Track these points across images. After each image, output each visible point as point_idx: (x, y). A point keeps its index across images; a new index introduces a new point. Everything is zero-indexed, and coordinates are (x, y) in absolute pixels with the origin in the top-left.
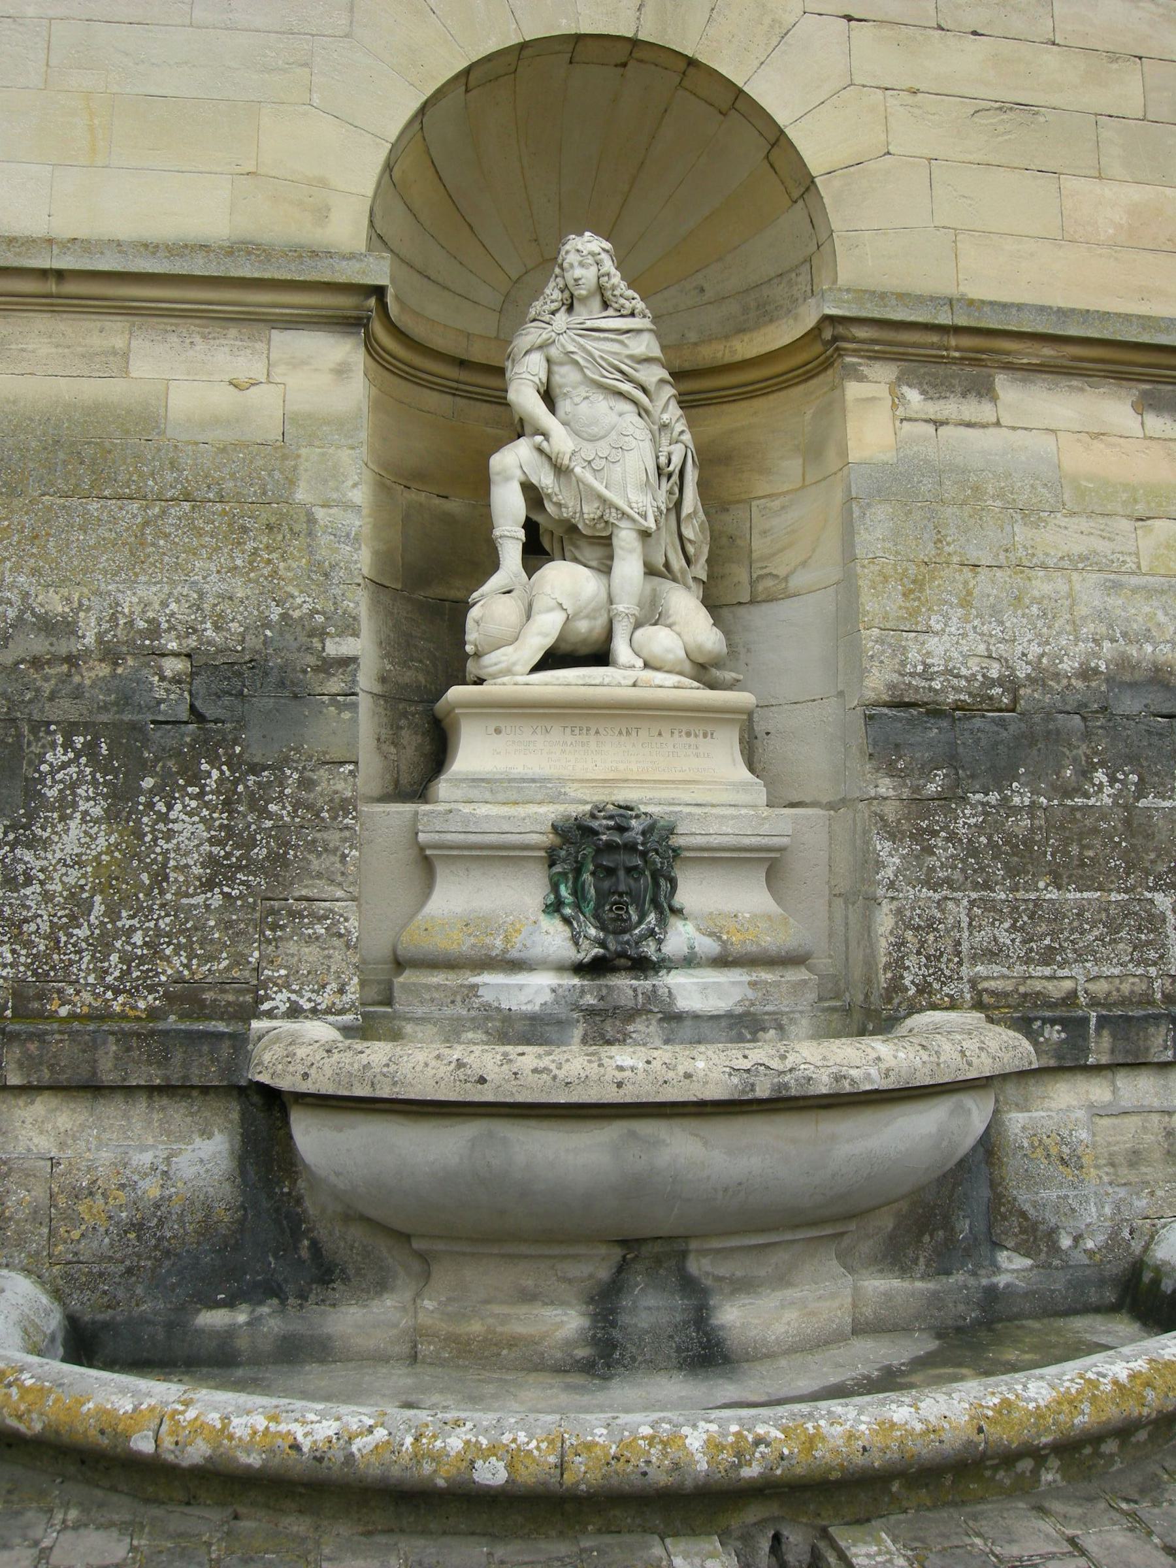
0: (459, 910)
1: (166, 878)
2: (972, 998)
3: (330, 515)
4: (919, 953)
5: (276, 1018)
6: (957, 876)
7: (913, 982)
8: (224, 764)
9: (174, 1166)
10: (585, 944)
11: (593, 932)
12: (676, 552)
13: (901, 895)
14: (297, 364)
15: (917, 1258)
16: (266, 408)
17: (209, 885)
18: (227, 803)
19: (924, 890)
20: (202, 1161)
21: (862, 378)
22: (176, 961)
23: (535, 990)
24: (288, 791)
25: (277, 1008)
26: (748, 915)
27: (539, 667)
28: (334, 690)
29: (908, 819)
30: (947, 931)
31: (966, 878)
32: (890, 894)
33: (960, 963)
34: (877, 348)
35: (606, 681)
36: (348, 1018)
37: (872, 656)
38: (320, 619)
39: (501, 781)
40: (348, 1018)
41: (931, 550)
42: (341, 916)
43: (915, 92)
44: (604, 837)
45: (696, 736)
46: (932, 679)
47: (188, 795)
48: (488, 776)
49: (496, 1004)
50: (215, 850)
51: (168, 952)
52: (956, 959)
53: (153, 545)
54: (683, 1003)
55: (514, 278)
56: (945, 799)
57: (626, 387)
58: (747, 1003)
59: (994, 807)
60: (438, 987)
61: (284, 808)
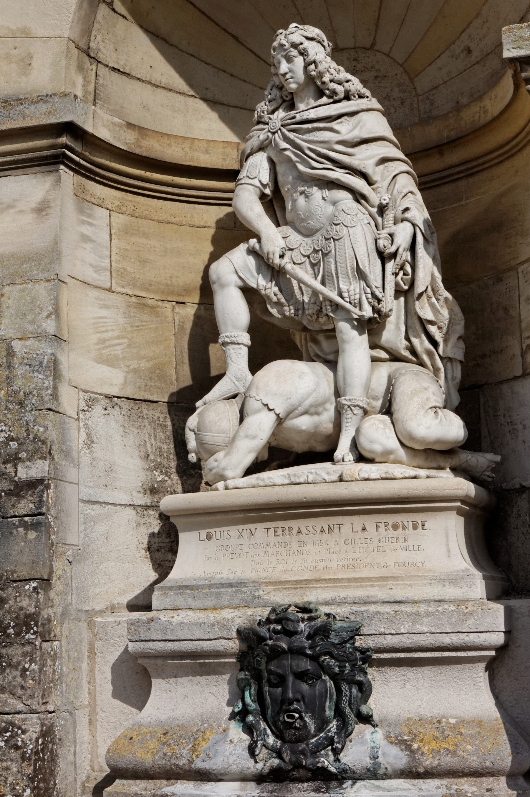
0: (163, 718)
3: (26, 347)
10: (262, 753)
11: (271, 740)
26: (453, 721)
27: (255, 468)
35: (311, 478)
38: (14, 445)
39: (202, 587)
42: (19, 728)
45: (404, 528)
48: (194, 583)
57: (339, 175)
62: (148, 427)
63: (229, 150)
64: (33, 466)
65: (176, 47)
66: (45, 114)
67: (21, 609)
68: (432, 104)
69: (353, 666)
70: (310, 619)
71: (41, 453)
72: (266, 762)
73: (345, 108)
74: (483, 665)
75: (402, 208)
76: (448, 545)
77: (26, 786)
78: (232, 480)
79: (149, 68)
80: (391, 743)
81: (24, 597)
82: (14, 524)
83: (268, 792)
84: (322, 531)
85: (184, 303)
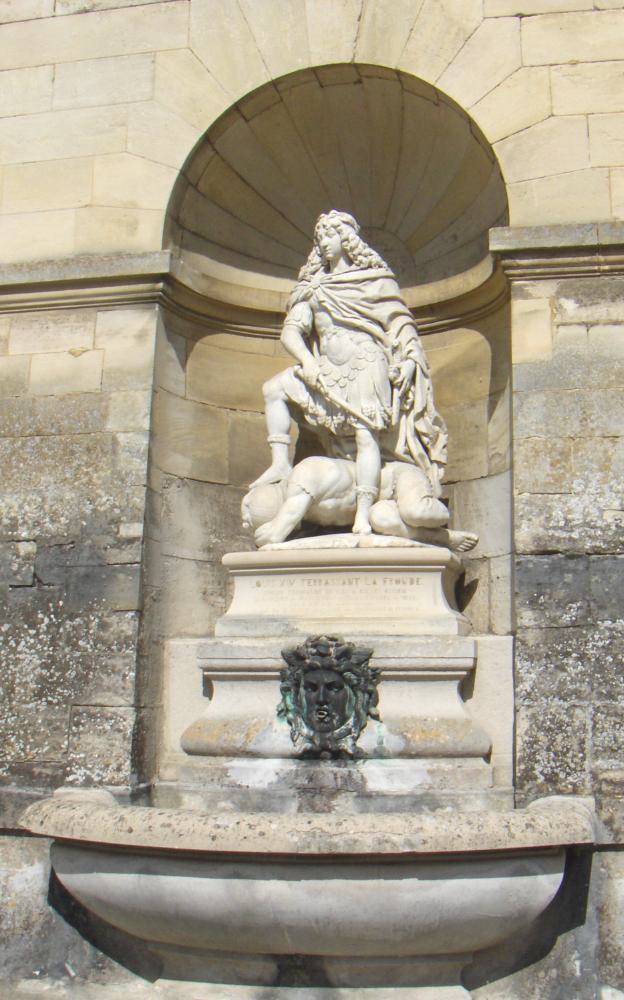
1: (13, 691)
2: (593, 786)
3: (128, 438)
4: (548, 749)
5: (76, 786)
6: (585, 688)
7: (541, 773)
8: (52, 613)
9: (10, 883)
13: (536, 704)
14: (113, 334)
15: (534, 989)
16: (89, 371)
17: (39, 695)
18: (53, 640)
19: (556, 699)
20: (26, 880)
22: (17, 747)
23: (261, 774)
24: (91, 632)
25: (77, 780)
27: (294, 535)
29: (545, 644)
30: (574, 733)
31: (592, 690)
32: (526, 703)
33: (583, 759)
34: (538, 271)
36: (121, 788)
37: (522, 516)
38: (117, 511)
40: (121, 788)
41: (576, 427)
43: (574, 63)
44: (308, 661)
45: (404, 583)
46: (572, 531)
47: (29, 635)
50: (44, 672)
51: (13, 740)
52: (581, 755)
53: (17, 467)
54: (372, 786)
56: (578, 626)
58: (427, 787)
59: (620, 632)
60: (204, 769)
61: (88, 643)
67: (122, 631)
69: (366, 680)
70: (337, 645)
72: (302, 745)
74: (457, 682)
75: (407, 350)
78: (275, 545)
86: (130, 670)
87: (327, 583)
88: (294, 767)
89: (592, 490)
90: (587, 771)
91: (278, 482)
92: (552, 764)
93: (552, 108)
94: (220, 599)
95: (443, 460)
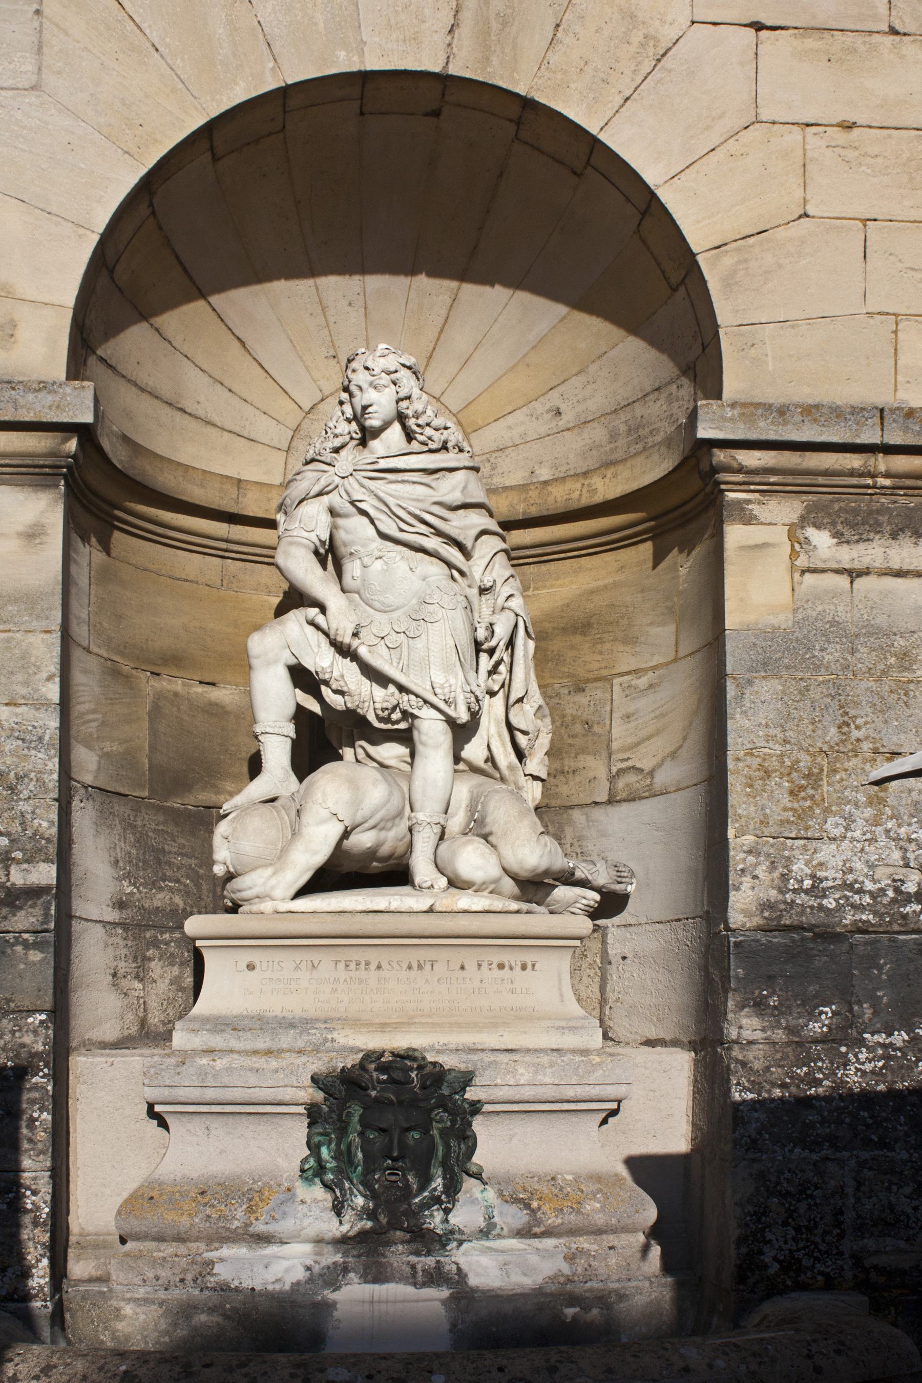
2: (855, 1276)
3: (17, 715)
4: (785, 1224)
7: (775, 1259)
11: (360, 1201)
12: (503, 745)
13: (765, 1156)
19: (797, 1150)
21: (750, 520)
26: (569, 1177)
27: (304, 891)
28: (20, 927)
33: (841, 1236)
34: (773, 479)
37: (743, 870)
43: (849, 126)
46: (825, 896)
49: (236, 1283)
55: (307, 406)
56: (833, 1041)
57: (433, 543)
59: (899, 1049)
62: (119, 827)
63: (227, 486)
64: (33, 870)
65: (170, 342)
66: (50, 407)
67: (23, 1045)
68: (493, 469)
70: (420, 1068)
71: (46, 854)
73: (443, 461)
76: (560, 989)
77: (41, 1255)
79: (136, 364)
80: (506, 1201)
81: (27, 1032)
82: (7, 941)
83: (353, 1256)
84: (410, 967)
85: (158, 675)
86: (41, 1110)
87: (379, 967)
88: (338, 1258)
89: (857, 834)
90: (846, 1256)
91: (273, 800)
92: (791, 1245)
93: (805, 201)
94: (137, 985)
95: (544, 776)
